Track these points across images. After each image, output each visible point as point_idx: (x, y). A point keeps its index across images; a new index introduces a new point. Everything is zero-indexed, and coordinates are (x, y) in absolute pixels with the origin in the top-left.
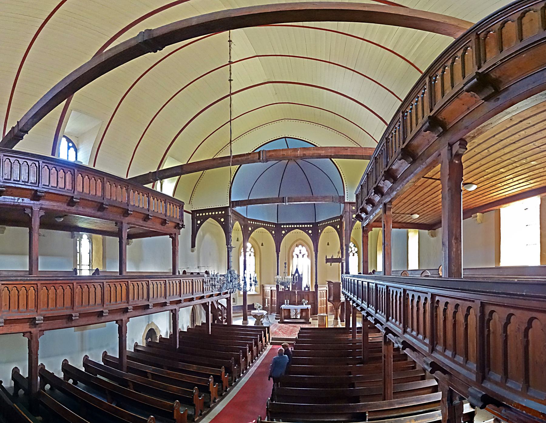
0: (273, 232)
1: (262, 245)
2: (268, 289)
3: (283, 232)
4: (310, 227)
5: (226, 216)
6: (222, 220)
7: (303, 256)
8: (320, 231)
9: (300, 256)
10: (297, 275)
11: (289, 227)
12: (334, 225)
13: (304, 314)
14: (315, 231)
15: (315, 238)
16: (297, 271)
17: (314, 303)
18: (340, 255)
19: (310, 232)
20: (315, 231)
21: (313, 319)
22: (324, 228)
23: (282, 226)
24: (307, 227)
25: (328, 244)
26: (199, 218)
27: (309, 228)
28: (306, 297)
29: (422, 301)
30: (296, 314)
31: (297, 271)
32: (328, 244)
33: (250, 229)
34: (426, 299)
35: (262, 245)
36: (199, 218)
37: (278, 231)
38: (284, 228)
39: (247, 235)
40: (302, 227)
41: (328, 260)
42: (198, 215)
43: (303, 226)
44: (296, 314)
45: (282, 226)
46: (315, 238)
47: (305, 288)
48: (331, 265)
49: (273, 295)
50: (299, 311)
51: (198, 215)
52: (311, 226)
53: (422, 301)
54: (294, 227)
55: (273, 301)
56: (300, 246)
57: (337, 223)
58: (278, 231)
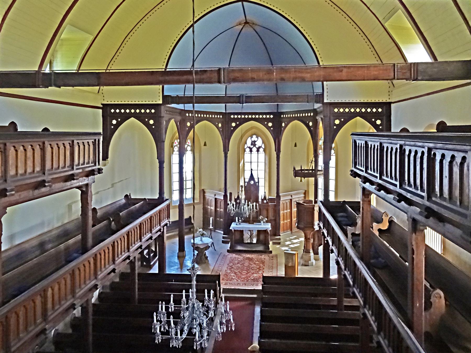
0: (220, 125)
1: (205, 145)
2: (210, 196)
3: (234, 124)
4: (270, 118)
5: (157, 117)
6: (151, 122)
7: (258, 151)
8: (283, 125)
9: (254, 149)
10: (252, 182)
11: (241, 118)
12: (305, 120)
13: (262, 237)
14: (277, 123)
15: (277, 133)
16: (252, 177)
17: (275, 220)
18: (313, 165)
19: (270, 124)
20: (277, 123)
21: (274, 243)
22: (291, 121)
23: (232, 116)
24: (266, 118)
25: (296, 146)
26: (115, 116)
27: (269, 120)
28: (265, 212)
29: (419, 155)
30: (251, 237)
31: (252, 177)
32: (296, 146)
33: (188, 124)
34: (423, 153)
35: (205, 145)
36: (115, 116)
37: (228, 125)
38: (234, 118)
39: (183, 133)
40: (259, 118)
41: (297, 174)
42: (113, 111)
43: (261, 116)
44: (251, 237)
45: (232, 116)
46: (277, 133)
47: (262, 200)
48: (301, 181)
49: (218, 205)
50: (255, 233)
51: (113, 111)
52: (272, 116)
53: (419, 155)
54: (248, 118)
55: (218, 213)
56: (254, 136)
57: (309, 120)
58: (228, 125)
